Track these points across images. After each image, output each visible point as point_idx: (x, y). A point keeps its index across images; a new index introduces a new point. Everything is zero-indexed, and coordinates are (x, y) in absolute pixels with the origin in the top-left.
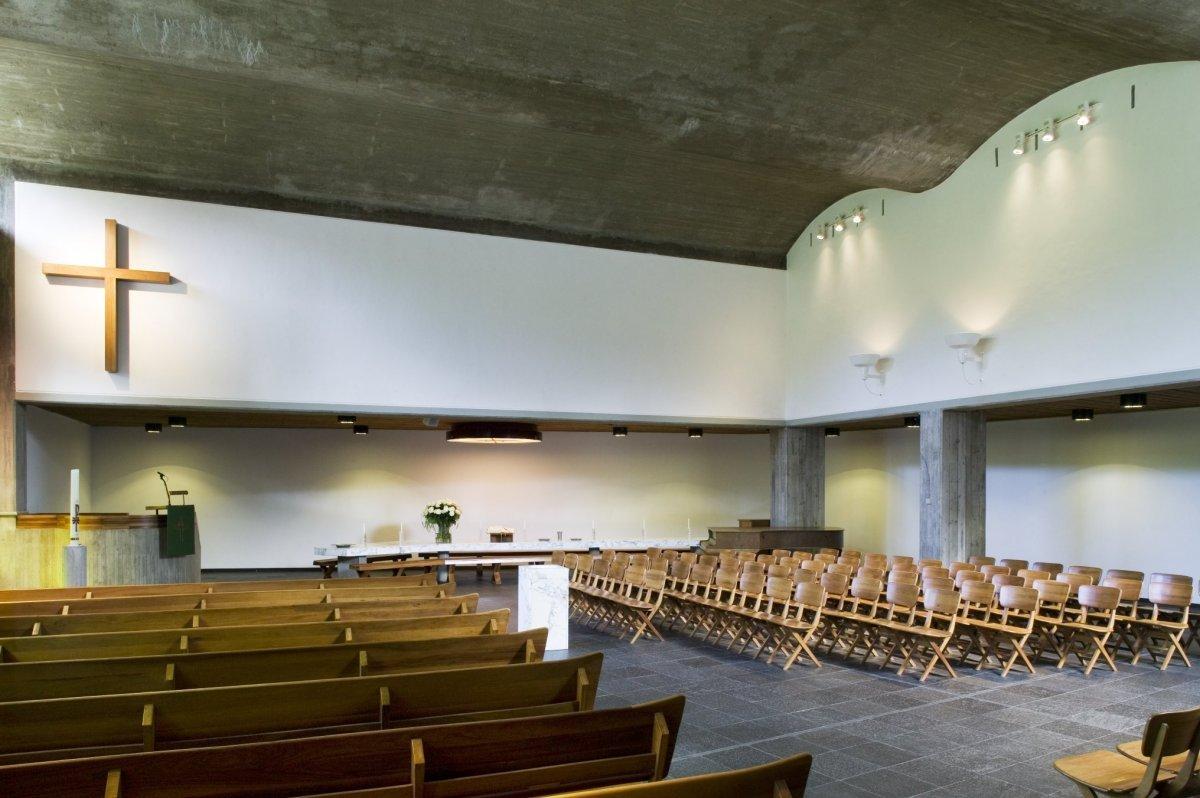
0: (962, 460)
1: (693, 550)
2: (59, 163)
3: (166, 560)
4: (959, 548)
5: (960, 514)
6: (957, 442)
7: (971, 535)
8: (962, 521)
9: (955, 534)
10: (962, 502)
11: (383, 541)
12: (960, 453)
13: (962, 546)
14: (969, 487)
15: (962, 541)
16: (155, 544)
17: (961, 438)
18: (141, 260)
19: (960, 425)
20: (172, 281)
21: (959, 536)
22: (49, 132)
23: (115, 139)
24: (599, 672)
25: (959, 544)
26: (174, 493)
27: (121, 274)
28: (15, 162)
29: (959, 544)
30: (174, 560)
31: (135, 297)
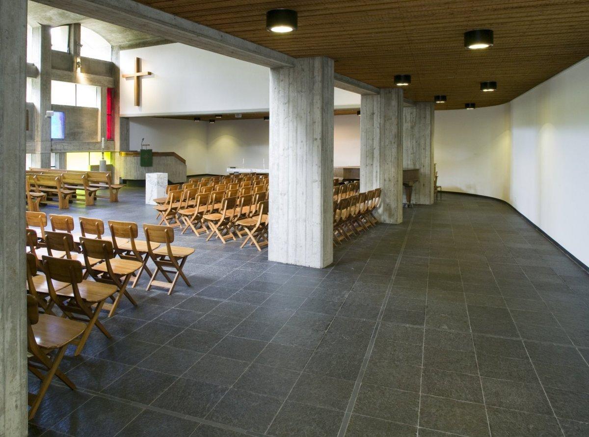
0: (376, 125)
1: (219, 422)
2: (127, 42)
3: (143, 168)
4: (374, 181)
5: (375, 159)
6: (373, 114)
7: (384, 174)
8: (376, 163)
9: (372, 172)
10: (377, 153)
11: (324, 225)
12: (375, 122)
13: (377, 180)
14: (382, 143)
15: (376, 177)
16: (139, 162)
17: (376, 112)
18: (145, 69)
19: (375, 103)
20: (150, 74)
21: (374, 174)
22: (120, 36)
23: (243, 183)
24: (29, 429)
25: (374, 179)
26: (144, 145)
27: (139, 74)
28: (120, 45)
29: (374, 179)
30: (147, 168)
31: (145, 82)
